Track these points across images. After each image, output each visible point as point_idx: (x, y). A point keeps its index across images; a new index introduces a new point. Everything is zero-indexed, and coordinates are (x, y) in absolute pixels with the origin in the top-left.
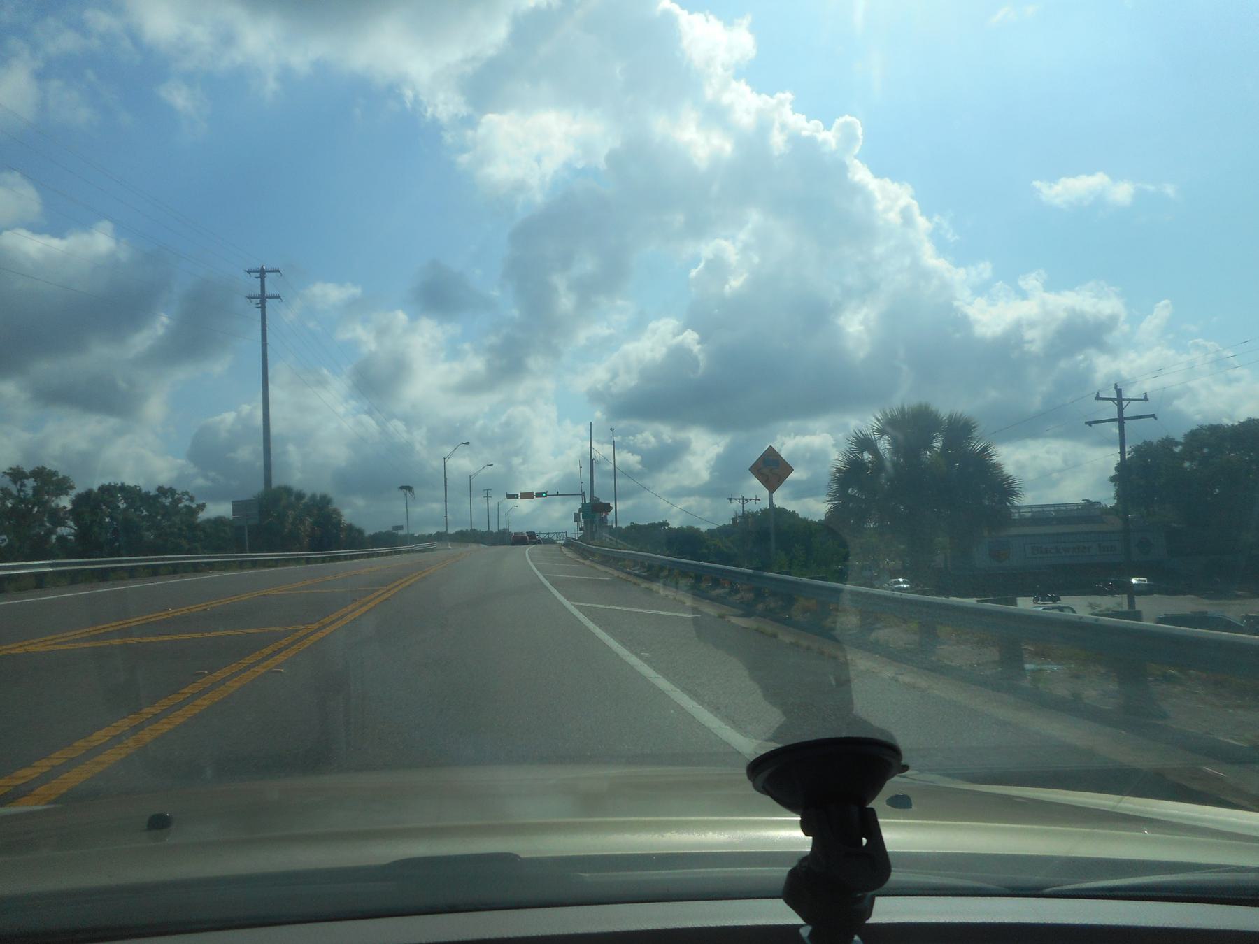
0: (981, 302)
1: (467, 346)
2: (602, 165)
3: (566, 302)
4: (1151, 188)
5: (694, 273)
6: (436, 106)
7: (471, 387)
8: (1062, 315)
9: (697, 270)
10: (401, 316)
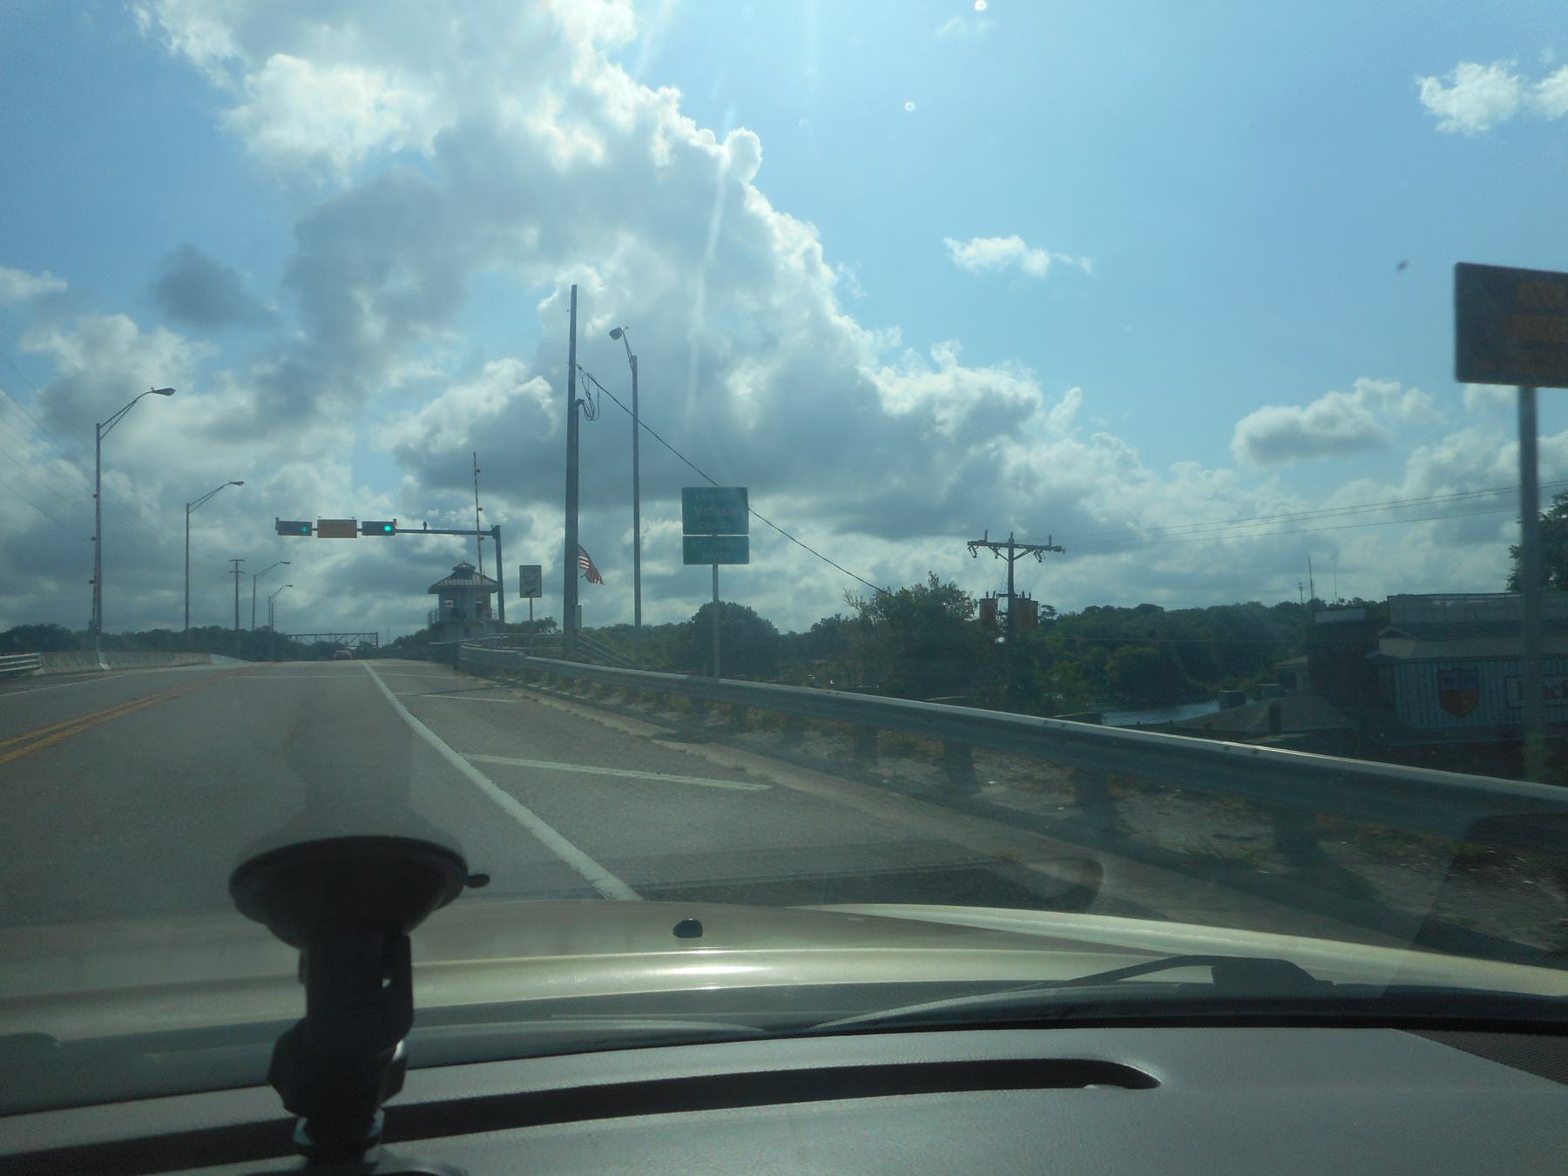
0: (888, 371)
1: (228, 374)
2: (429, 149)
3: (373, 327)
4: (1067, 259)
5: (544, 304)
6: (186, 38)
7: (229, 431)
8: (977, 395)
9: (549, 300)
10: (126, 327)
